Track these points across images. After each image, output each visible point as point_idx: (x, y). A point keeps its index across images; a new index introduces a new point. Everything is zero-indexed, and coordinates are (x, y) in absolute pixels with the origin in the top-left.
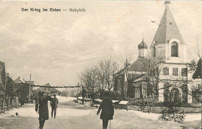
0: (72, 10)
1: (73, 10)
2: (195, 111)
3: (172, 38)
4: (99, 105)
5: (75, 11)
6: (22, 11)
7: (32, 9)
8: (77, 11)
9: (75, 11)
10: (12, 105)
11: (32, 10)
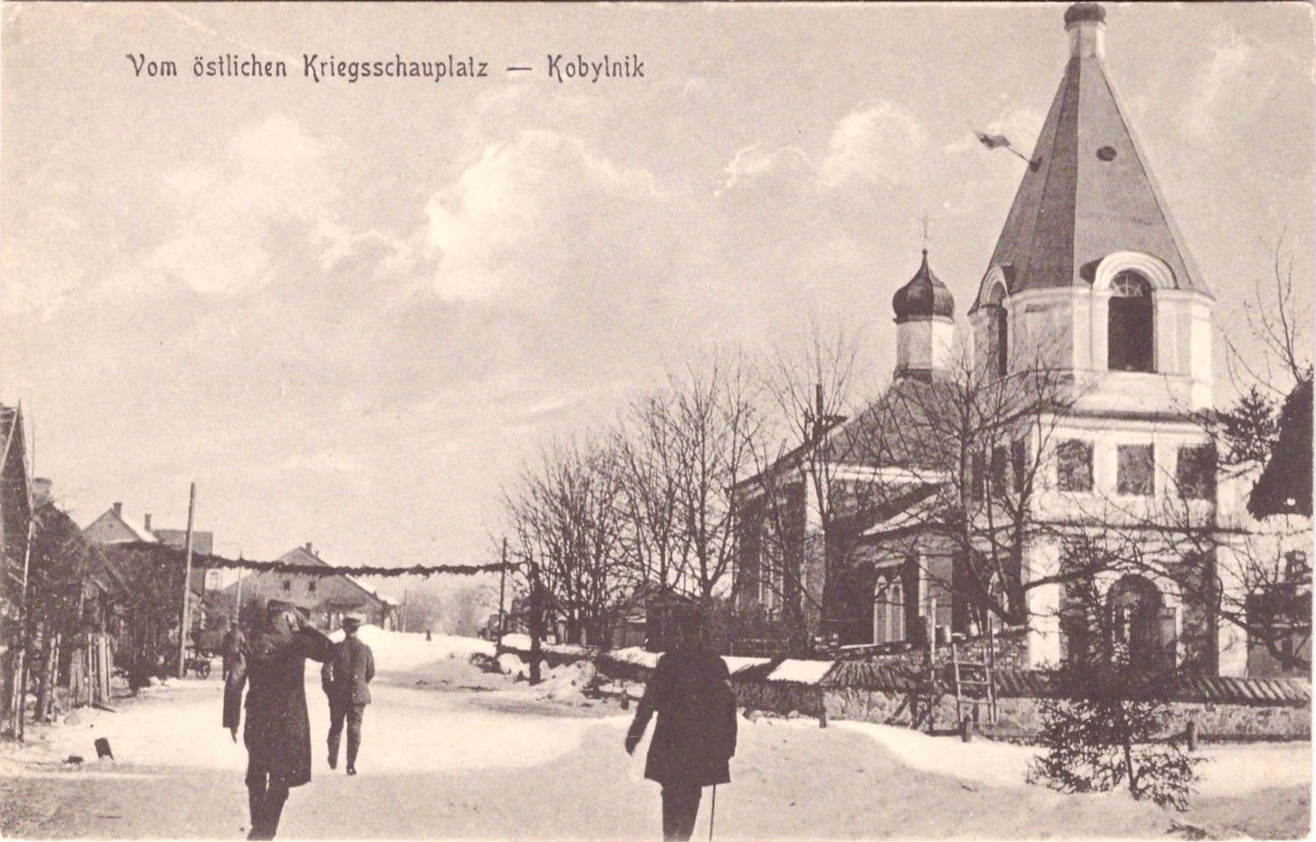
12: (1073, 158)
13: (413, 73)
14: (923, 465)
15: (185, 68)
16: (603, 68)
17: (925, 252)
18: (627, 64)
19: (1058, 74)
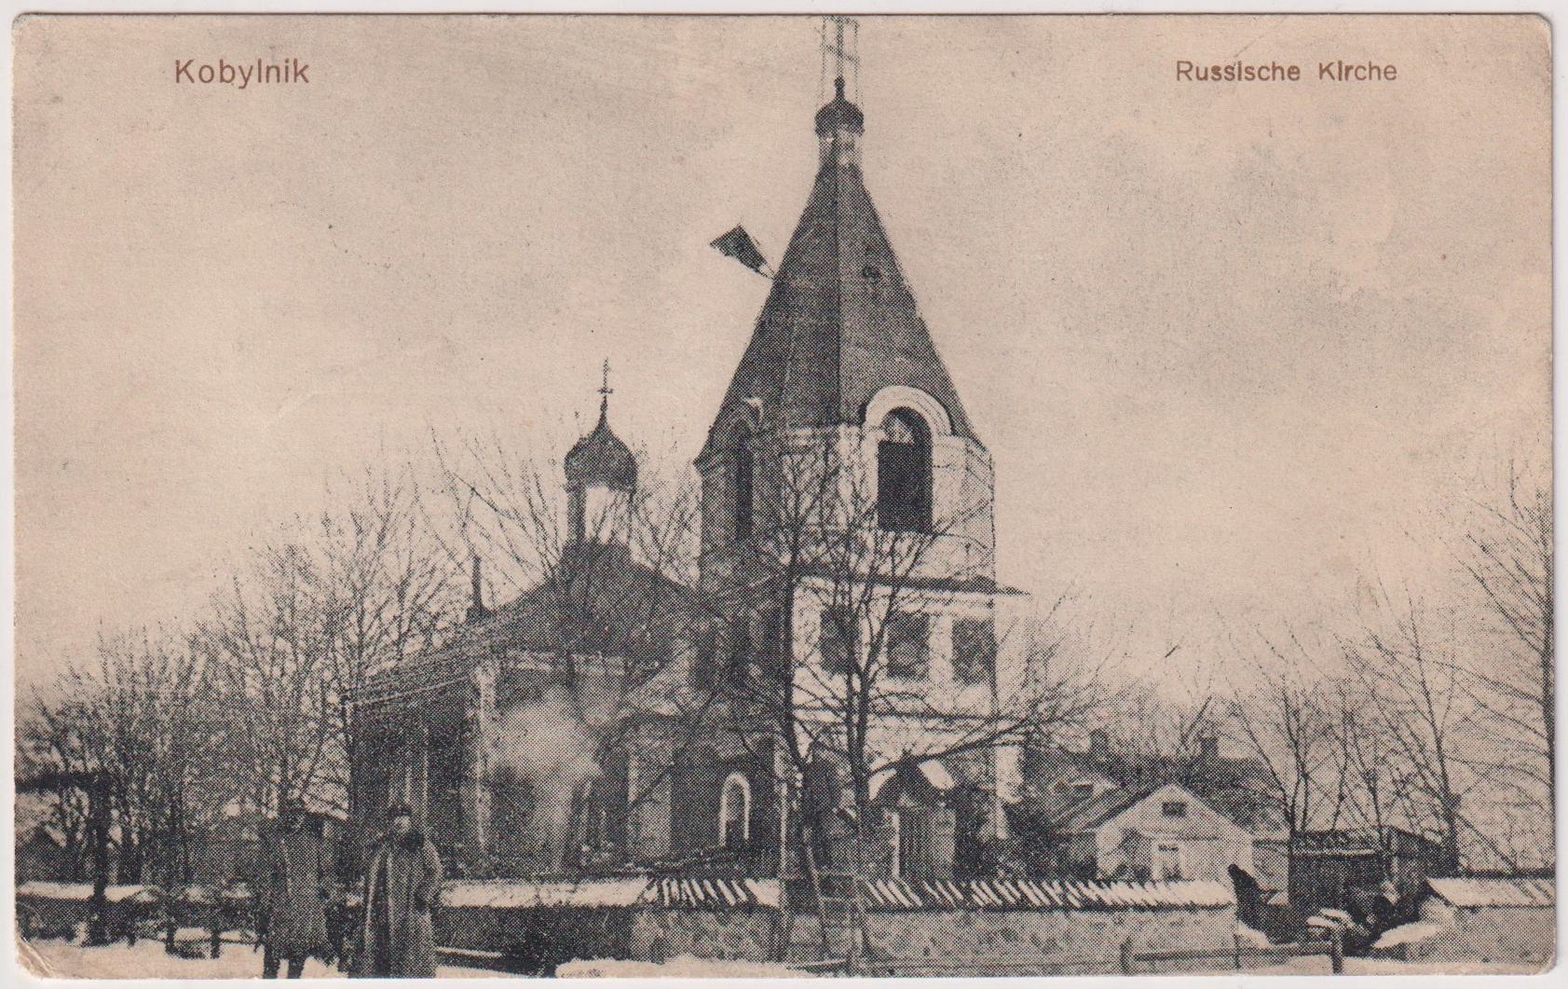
0: (193, 70)
1: (206, 74)
2: (1183, 946)
3: (885, 381)
4: (744, 898)
5: (222, 80)
6: (1179, 63)
8: (239, 80)
11: (1326, 74)
13: (1216, 70)
14: (706, 943)
15: (1309, 71)
16: (255, 72)
18: (287, 68)
19: (967, 402)
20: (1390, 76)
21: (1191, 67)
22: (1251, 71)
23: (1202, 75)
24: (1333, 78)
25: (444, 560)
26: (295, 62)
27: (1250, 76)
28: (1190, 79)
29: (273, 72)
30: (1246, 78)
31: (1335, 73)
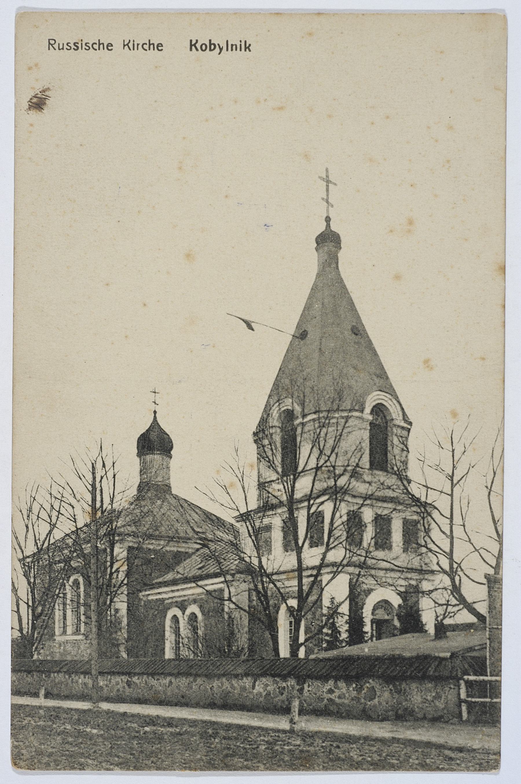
0: (198, 45)
5: (210, 50)
6: (49, 40)
7: (195, 45)
8: (217, 50)
9: (210, 50)
10: (222, 585)
12: (500, 632)
17: (155, 412)
18: (241, 45)
20: (110, 48)
21: (55, 42)
22: (77, 44)
23: (61, 47)
24: (130, 50)
25: (329, 484)
26: (245, 42)
27: (87, 48)
28: (55, 49)
29: (234, 47)
30: (85, 49)
31: (131, 47)
